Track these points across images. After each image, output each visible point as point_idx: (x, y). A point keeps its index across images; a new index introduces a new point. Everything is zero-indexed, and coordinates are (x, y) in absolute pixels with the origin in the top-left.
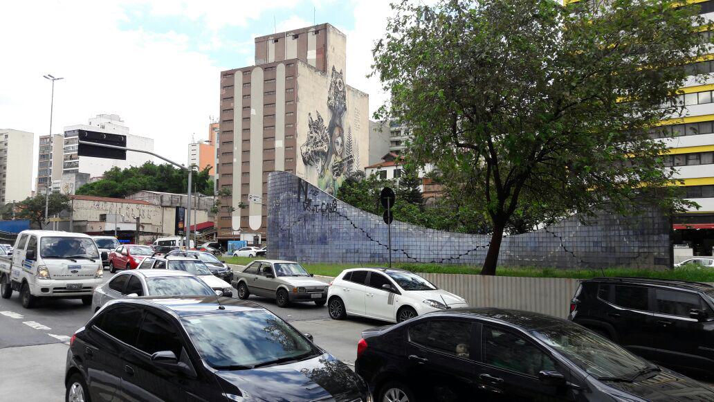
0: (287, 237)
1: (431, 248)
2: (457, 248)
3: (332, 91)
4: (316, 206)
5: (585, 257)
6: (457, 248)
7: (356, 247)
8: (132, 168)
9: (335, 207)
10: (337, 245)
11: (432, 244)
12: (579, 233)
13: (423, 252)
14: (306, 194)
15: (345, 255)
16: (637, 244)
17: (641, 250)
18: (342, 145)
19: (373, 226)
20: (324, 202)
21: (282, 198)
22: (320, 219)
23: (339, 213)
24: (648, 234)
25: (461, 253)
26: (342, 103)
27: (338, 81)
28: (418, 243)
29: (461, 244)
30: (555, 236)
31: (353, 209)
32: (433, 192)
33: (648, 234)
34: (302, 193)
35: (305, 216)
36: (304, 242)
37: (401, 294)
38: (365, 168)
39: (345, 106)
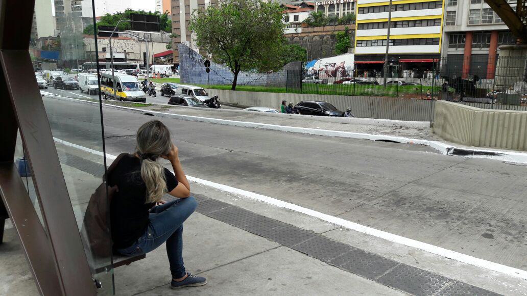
8: (118, 14)
14: (192, 54)
32: (307, 33)
36: (193, 75)
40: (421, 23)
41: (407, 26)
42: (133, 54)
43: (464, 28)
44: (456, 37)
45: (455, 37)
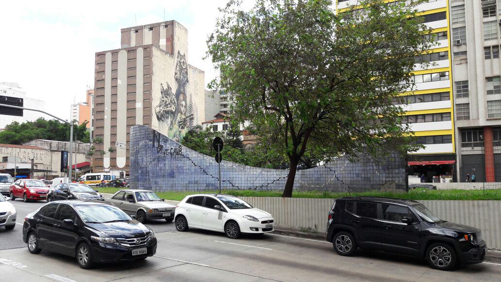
0: (145, 173)
1: (249, 179)
2: (266, 179)
4: (167, 150)
6: (266, 179)
7: (196, 179)
9: (180, 151)
10: (181, 178)
12: (346, 169)
14: (159, 141)
15: (187, 185)
16: (384, 175)
17: (387, 180)
18: (185, 107)
19: (208, 164)
21: (141, 144)
22: (169, 159)
23: (183, 155)
25: (269, 182)
27: (182, 61)
28: (240, 176)
29: (269, 176)
30: (331, 170)
31: (194, 152)
33: (392, 168)
35: (158, 158)
36: (158, 176)
37: (227, 212)
38: (202, 123)
39: (187, 79)
40: (425, 119)
43: (482, 122)
44: (469, 134)
45: (469, 134)
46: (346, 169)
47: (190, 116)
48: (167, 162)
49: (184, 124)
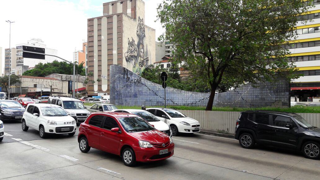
2: (195, 99)
3: (139, 28)
4: (132, 80)
5: (252, 102)
6: (195, 99)
7: (150, 99)
8: (48, 63)
11: (184, 97)
13: (180, 101)
16: (274, 96)
17: (276, 99)
18: (143, 53)
19: (158, 89)
20: (136, 78)
21: (116, 77)
22: (134, 86)
24: (280, 92)
25: (197, 101)
26: (143, 34)
29: (197, 97)
30: (238, 93)
32: (184, 74)
34: (125, 74)
35: (127, 85)
36: (127, 97)
38: (154, 63)
39: (144, 35)
40: (303, 59)
41: (302, 60)
42: (57, 89)
46: (249, 92)
47: (146, 59)
48: (132, 88)
49: (143, 64)
